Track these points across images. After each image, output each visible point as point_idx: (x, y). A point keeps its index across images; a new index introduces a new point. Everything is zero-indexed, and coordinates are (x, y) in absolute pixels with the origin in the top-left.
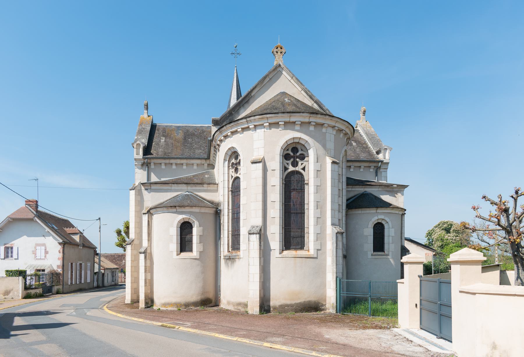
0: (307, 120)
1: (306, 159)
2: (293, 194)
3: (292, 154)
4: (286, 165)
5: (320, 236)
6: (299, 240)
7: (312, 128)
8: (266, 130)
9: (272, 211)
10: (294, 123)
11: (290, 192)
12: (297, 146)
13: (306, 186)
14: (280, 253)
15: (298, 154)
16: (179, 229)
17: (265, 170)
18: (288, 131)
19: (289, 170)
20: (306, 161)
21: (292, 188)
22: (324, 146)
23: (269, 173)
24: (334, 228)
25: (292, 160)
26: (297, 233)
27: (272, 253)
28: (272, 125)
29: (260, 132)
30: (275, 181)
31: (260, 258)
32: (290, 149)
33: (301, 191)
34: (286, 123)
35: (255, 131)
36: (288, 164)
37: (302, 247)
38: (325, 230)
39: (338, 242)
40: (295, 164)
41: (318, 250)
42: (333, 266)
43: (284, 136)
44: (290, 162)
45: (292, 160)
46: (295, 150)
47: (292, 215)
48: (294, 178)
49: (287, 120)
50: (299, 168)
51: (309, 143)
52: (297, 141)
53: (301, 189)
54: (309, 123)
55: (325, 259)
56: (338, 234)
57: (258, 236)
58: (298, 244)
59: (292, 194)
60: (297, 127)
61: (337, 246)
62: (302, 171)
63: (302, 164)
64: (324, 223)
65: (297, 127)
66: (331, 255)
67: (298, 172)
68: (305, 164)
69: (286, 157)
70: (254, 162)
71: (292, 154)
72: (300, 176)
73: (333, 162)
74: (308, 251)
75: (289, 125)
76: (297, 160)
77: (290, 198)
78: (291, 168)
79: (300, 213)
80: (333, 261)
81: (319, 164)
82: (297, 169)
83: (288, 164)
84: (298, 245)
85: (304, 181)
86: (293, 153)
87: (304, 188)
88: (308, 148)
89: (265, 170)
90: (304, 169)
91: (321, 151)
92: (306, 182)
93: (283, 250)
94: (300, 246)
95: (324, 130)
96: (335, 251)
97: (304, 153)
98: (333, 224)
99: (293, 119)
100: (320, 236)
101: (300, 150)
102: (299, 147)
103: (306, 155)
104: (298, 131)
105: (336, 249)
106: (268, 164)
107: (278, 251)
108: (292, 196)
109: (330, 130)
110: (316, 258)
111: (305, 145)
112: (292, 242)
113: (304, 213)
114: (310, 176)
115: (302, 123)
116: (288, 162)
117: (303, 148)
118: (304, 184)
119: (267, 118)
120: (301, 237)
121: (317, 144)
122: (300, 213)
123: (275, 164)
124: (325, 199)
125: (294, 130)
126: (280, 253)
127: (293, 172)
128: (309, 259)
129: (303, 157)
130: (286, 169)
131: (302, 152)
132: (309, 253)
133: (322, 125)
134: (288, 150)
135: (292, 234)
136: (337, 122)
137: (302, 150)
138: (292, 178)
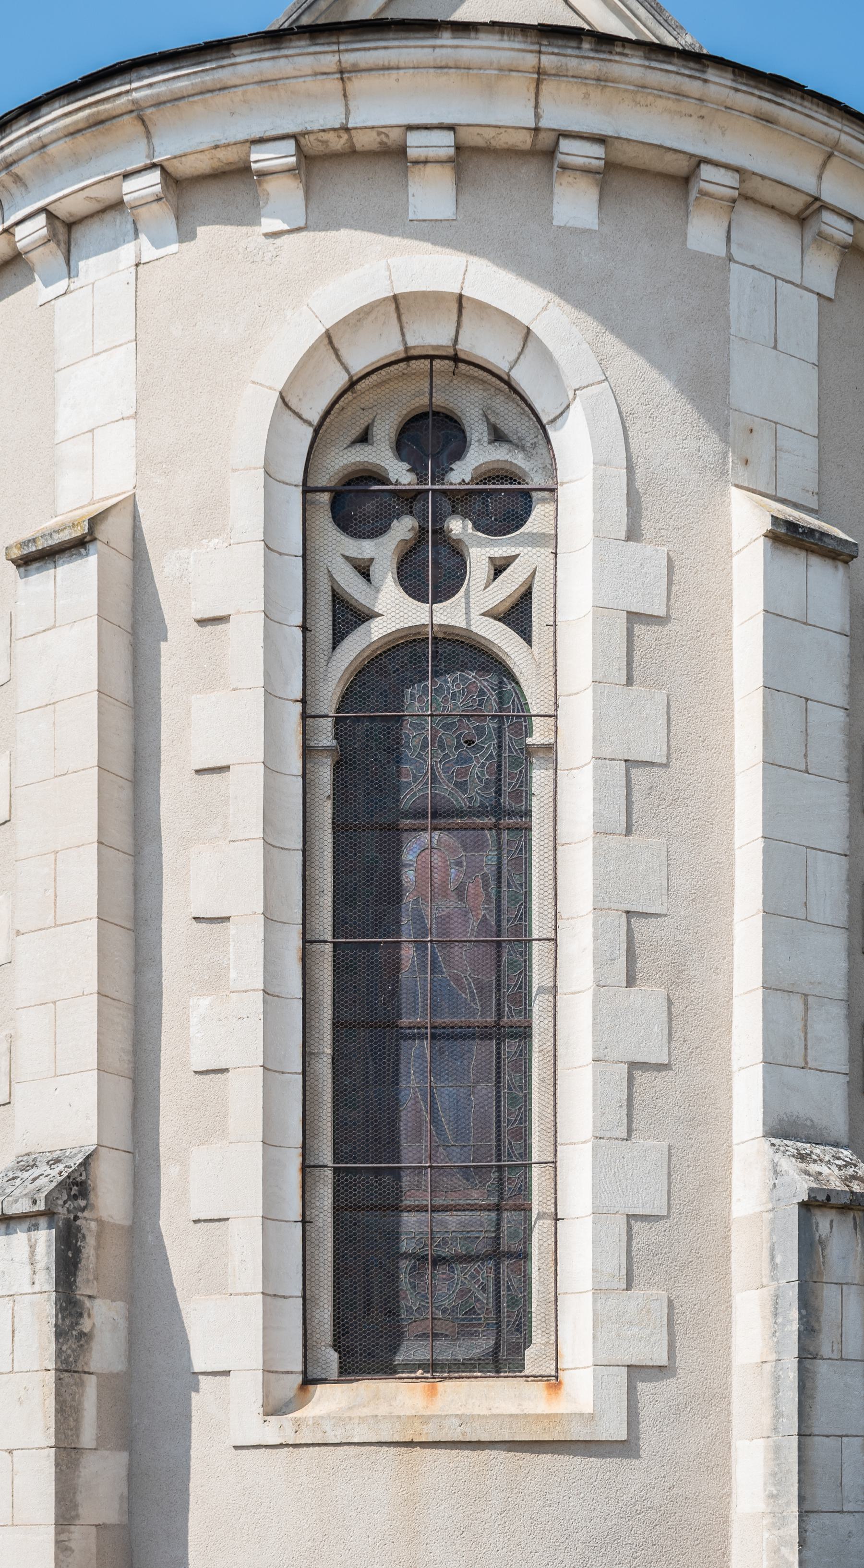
0: (508, 112)
1: (538, 519)
2: (424, 857)
3: (401, 474)
4: (353, 586)
5: (657, 1243)
6: (474, 1279)
7: (575, 205)
8: (149, 252)
9: (201, 1005)
10: (392, 154)
11: (392, 835)
12: (440, 400)
13: (540, 777)
14: (274, 1409)
15: (461, 474)
16: (847, 659)
17: (135, 626)
18: (344, 234)
19: (377, 630)
20: (537, 540)
21: (407, 800)
22: (707, 390)
23: (174, 658)
24: (788, 1165)
25: (403, 528)
26: (452, 1220)
27: (204, 1403)
28: (208, 189)
29: (107, 270)
30: (233, 727)
31: (67, 1454)
32: (385, 431)
33: (501, 816)
34: (315, 160)
35: (70, 271)
36: (364, 570)
37: (503, 1356)
38: (718, 1184)
39: (829, 1296)
40: (432, 571)
41: (636, 1372)
42: (779, 1522)
43: (305, 289)
44: (382, 552)
45: (403, 528)
46: (431, 434)
47: (415, 1056)
48: (422, 704)
49: (321, 115)
50: (470, 610)
51: (546, 355)
52: (432, 334)
53: (498, 811)
54: (543, 152)
55: (717, 1464)
56: (823, 1222)
57: (44, 1239)
58: (466, 1322)
59: (408, 856)
60: (431, 195)
61: (809, 1329)
62: (501, 638)
63: (499, 568)
64: (706, 1114)
65: (431, 195)
66: (766, 1420)
67: (461, 652)
68: (528, 560)
69: (353, 503)
70: (35, 558)
71: (401, 474)
72: (486, 682)
73: (788, 537)
74: (553, 1381)
75: (343, 169)
76: (457, 526)
77: (393, 892)
78: (394, 610)
79: (485, 1033)
80: (775, 1477)
81: (650, 555)
82: (449, 614)
83: (364, 570)
84: (466, 1328)
85: (522, 722)
86: (413, 460)
87: (523, 792)
88: (545, 408)
89: (135, 626)
90: (518, 614)
91: (675, 434)
92: (538, 736)
93: (308, 1381)
94: (482, 1344)
95: (704, 233)
96: (792, 1376)
97: (518, 460)
98: (782, 1129)
99: (379, 108)
100: (657, 1243)
101: (477, 432)
102: (469, 405)
103: (536, 480)
104: (432, 232)
105: (807, 1356)
106: (165, 570)
107: (247, 1389)
108: (409, 876)
109: (769, 242)
110: (626, 1448)
111: (522, 377)
112: (409, 1300)
113: (524, 1034)
114: (569, 681)
115: (470, 157)
116: (366, 548)
117: (511, 420)
118: (525, 757)
119: (138, 112)
120: (496, 1255)
121: (629, 363)
122: (485, 1033)
123: (228, 563)
124: (715, 893)
125: (394, 222)
126: (274, 1409)
127: (409, 654)
128: (546, 1459)
129: (506, 505)
130: (348, 616)
131: (499, 454)
132: (561, 1406)
133: (680, 179)
134: (364, 438)
135: (412, 1223)
136: (830, 153)
137: (498, 436)
138: (418, 703)
